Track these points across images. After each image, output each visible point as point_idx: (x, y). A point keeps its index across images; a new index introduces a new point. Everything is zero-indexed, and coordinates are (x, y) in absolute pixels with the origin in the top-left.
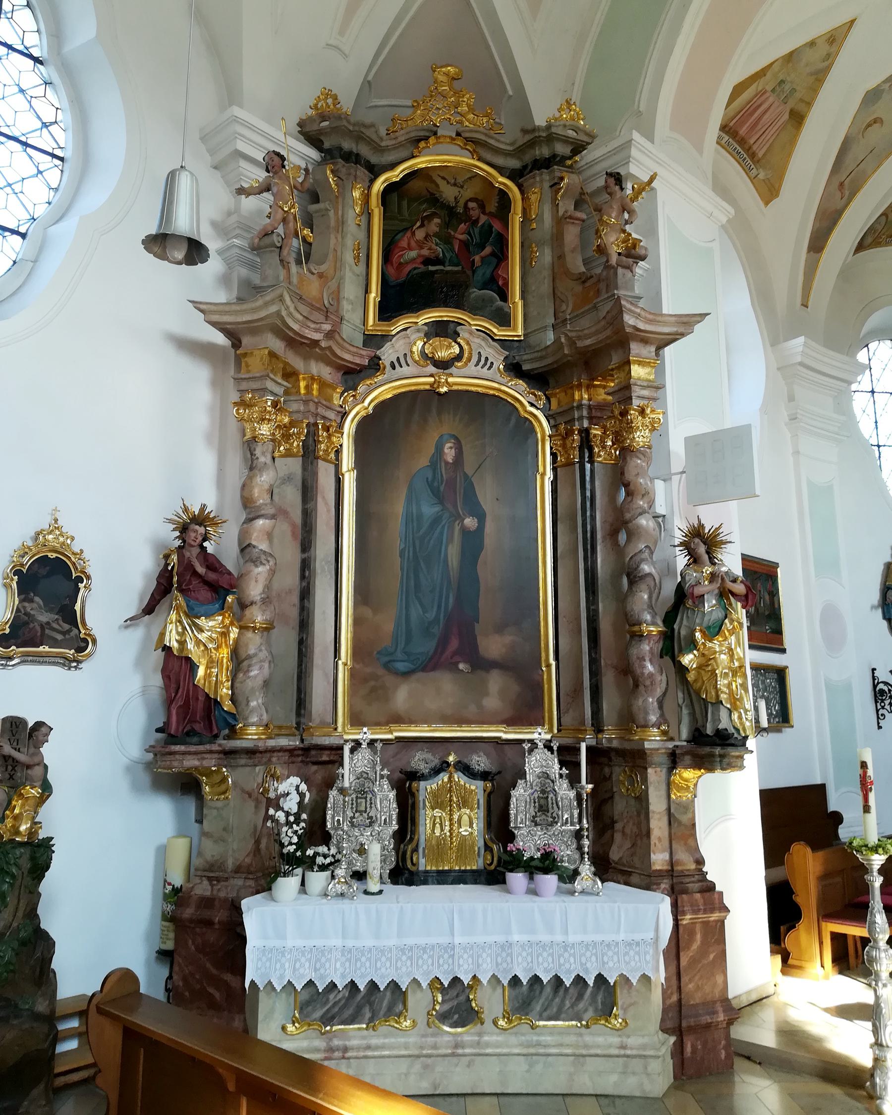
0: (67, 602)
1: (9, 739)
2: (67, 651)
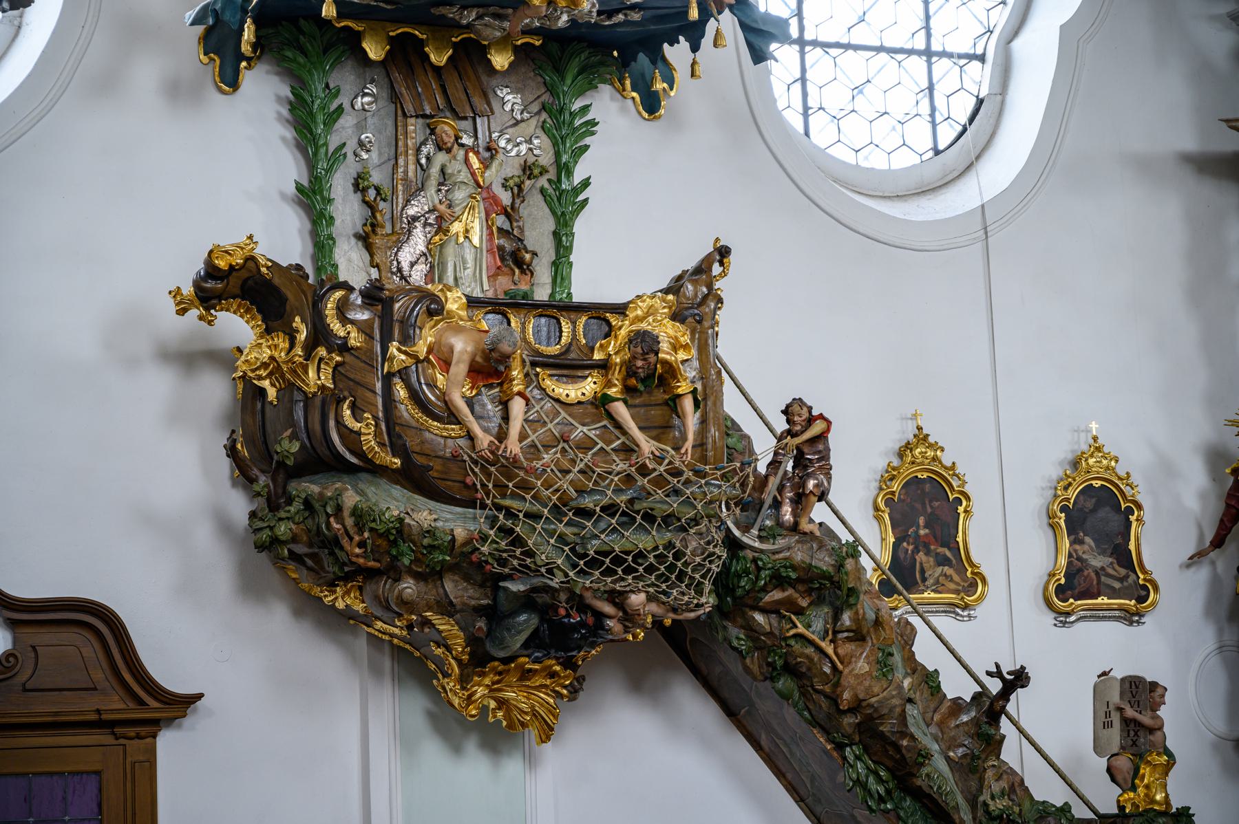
0: (1119, 540)
1: (1129, 702)
2: (1127, 602)
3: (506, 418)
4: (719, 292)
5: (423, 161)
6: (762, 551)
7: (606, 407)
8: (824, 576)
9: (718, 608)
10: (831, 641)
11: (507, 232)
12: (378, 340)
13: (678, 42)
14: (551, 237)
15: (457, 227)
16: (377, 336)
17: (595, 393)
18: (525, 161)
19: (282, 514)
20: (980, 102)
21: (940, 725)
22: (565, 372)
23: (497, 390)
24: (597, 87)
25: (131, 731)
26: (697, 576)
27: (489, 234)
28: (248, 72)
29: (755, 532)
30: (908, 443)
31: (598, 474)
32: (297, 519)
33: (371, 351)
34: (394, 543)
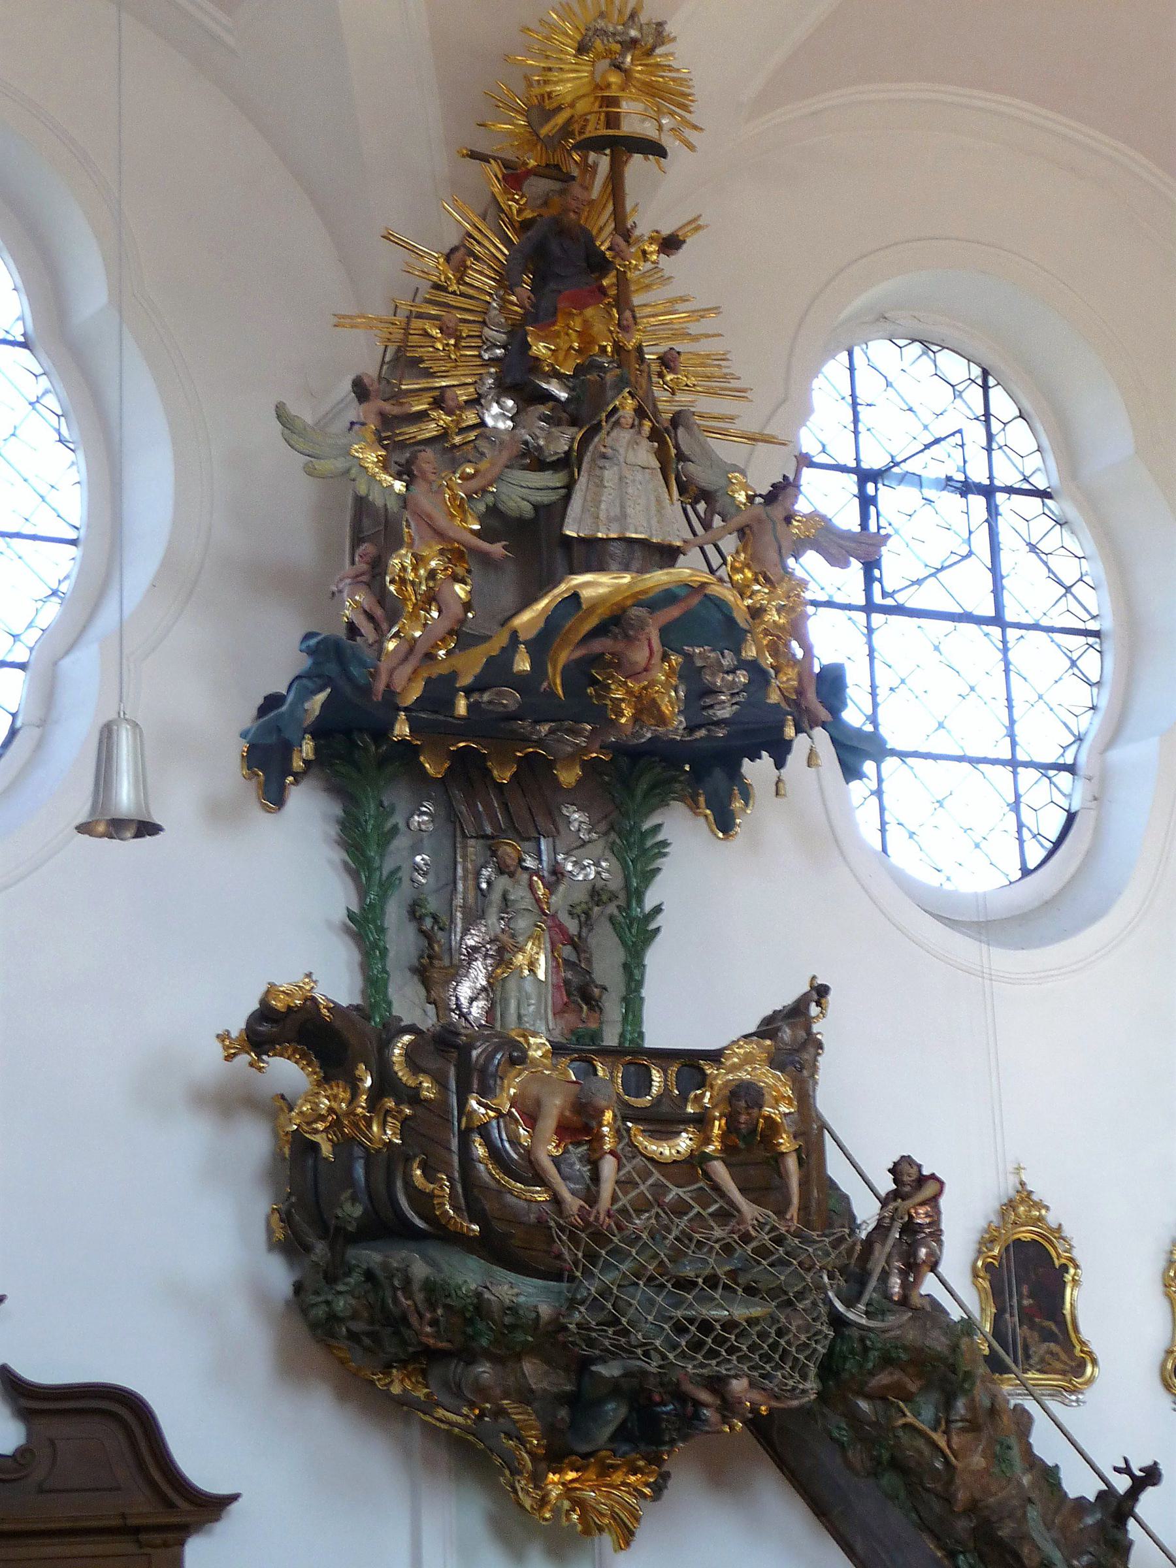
3: (596, 1178)
4: (819, 1037)
5: (484, 886)
6: (869, 1329)
7: (704, 1167)
8: (940, 1358)
9: (822, 1396)
10: (944, 1432)
11: (574, 963)
12: (454, 1090)
13: (760, 758)
14: (621, 969)
15: (520, 959)
16: (453, 1085)
17: (692, 1150)
18: (594, 887)
19: (341, 1288)
20: (1071, 818)
21: (1064, 1528)
22: (658, 1127)
23: (585, 1147)
24: (311, 652)
25: (157, 1538)
26: (801, 1357)
27: (556, 967)
28: (293, 787)
29: (862, 1307)
30: (1011, 1201)
31: (698, 1241)
32: (356, 1293)
33: (444, 1103)
34: (470, 1322)
